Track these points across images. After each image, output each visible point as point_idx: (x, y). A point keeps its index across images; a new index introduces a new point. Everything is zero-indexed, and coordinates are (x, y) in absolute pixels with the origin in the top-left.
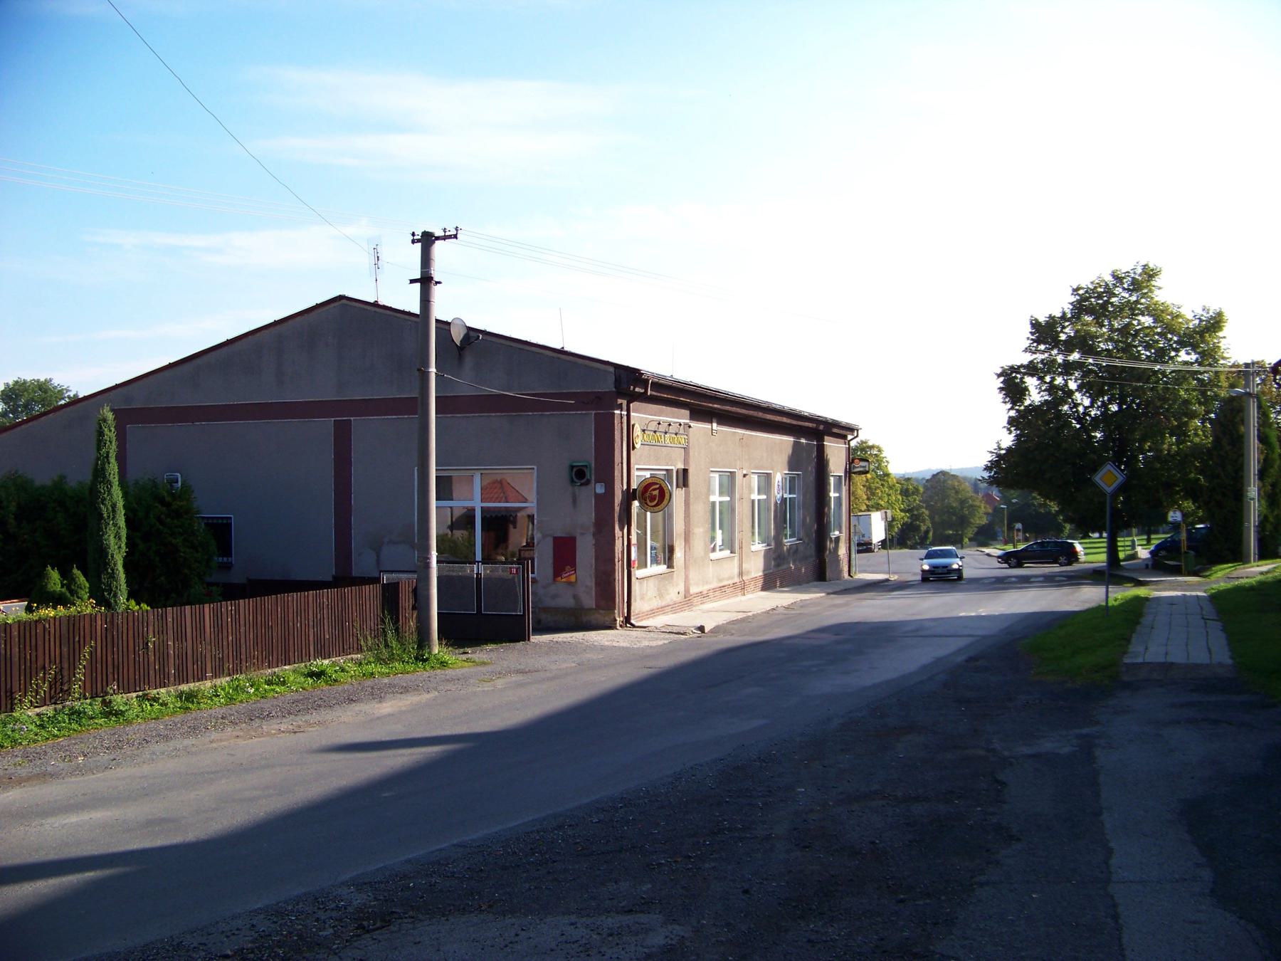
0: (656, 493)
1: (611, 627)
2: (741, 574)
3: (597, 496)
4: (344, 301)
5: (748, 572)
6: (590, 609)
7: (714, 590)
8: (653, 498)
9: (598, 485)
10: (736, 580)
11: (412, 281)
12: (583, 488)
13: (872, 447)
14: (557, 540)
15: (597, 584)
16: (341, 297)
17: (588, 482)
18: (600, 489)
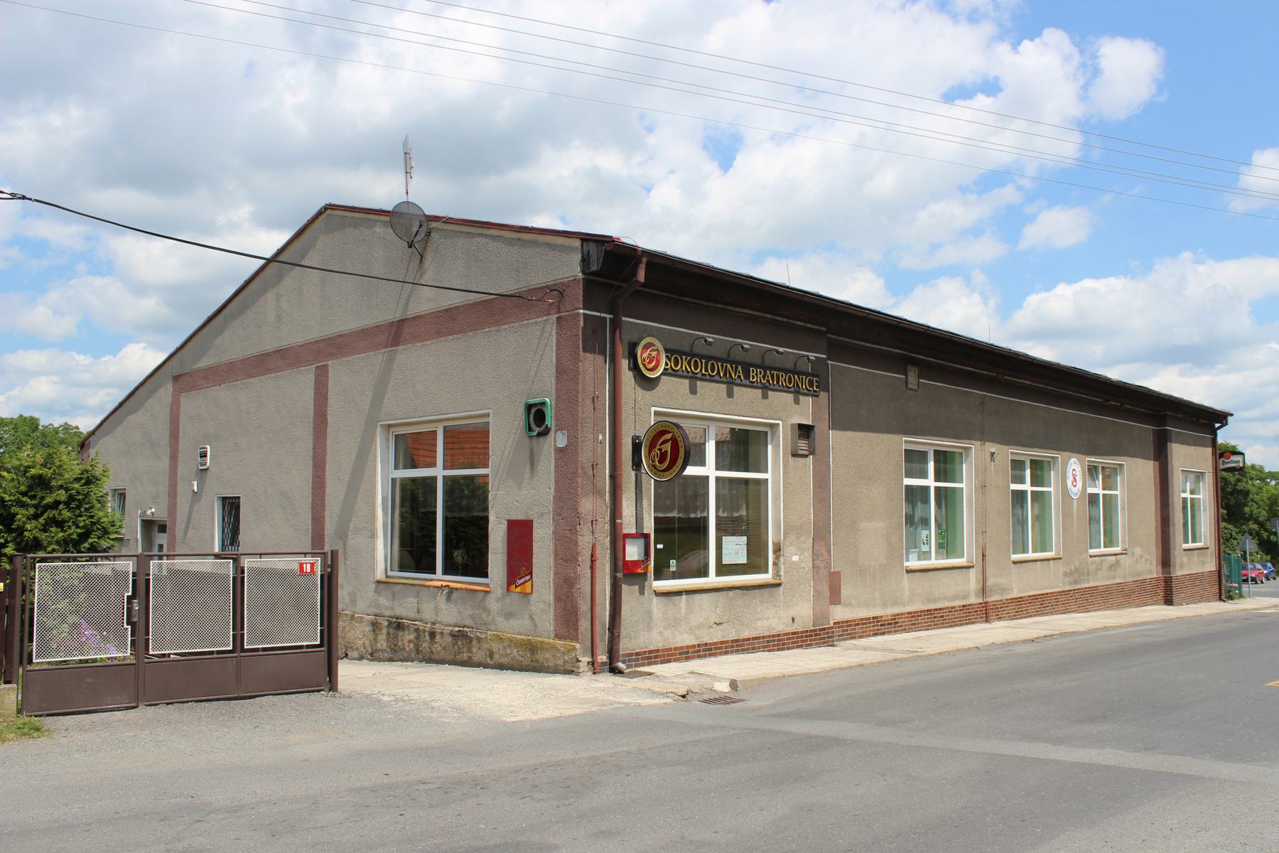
0: (668, 447)
1: (577, 674)
2: (984, 591)
3: (559, 451)
4: (329, 212)
6: (1214, 441)
7: (912, 615)
10: (973, 600)
12: (542, 439)
15: (558, 599)
16: (329, 207)
17: (545, 433)
18: (562, 441)
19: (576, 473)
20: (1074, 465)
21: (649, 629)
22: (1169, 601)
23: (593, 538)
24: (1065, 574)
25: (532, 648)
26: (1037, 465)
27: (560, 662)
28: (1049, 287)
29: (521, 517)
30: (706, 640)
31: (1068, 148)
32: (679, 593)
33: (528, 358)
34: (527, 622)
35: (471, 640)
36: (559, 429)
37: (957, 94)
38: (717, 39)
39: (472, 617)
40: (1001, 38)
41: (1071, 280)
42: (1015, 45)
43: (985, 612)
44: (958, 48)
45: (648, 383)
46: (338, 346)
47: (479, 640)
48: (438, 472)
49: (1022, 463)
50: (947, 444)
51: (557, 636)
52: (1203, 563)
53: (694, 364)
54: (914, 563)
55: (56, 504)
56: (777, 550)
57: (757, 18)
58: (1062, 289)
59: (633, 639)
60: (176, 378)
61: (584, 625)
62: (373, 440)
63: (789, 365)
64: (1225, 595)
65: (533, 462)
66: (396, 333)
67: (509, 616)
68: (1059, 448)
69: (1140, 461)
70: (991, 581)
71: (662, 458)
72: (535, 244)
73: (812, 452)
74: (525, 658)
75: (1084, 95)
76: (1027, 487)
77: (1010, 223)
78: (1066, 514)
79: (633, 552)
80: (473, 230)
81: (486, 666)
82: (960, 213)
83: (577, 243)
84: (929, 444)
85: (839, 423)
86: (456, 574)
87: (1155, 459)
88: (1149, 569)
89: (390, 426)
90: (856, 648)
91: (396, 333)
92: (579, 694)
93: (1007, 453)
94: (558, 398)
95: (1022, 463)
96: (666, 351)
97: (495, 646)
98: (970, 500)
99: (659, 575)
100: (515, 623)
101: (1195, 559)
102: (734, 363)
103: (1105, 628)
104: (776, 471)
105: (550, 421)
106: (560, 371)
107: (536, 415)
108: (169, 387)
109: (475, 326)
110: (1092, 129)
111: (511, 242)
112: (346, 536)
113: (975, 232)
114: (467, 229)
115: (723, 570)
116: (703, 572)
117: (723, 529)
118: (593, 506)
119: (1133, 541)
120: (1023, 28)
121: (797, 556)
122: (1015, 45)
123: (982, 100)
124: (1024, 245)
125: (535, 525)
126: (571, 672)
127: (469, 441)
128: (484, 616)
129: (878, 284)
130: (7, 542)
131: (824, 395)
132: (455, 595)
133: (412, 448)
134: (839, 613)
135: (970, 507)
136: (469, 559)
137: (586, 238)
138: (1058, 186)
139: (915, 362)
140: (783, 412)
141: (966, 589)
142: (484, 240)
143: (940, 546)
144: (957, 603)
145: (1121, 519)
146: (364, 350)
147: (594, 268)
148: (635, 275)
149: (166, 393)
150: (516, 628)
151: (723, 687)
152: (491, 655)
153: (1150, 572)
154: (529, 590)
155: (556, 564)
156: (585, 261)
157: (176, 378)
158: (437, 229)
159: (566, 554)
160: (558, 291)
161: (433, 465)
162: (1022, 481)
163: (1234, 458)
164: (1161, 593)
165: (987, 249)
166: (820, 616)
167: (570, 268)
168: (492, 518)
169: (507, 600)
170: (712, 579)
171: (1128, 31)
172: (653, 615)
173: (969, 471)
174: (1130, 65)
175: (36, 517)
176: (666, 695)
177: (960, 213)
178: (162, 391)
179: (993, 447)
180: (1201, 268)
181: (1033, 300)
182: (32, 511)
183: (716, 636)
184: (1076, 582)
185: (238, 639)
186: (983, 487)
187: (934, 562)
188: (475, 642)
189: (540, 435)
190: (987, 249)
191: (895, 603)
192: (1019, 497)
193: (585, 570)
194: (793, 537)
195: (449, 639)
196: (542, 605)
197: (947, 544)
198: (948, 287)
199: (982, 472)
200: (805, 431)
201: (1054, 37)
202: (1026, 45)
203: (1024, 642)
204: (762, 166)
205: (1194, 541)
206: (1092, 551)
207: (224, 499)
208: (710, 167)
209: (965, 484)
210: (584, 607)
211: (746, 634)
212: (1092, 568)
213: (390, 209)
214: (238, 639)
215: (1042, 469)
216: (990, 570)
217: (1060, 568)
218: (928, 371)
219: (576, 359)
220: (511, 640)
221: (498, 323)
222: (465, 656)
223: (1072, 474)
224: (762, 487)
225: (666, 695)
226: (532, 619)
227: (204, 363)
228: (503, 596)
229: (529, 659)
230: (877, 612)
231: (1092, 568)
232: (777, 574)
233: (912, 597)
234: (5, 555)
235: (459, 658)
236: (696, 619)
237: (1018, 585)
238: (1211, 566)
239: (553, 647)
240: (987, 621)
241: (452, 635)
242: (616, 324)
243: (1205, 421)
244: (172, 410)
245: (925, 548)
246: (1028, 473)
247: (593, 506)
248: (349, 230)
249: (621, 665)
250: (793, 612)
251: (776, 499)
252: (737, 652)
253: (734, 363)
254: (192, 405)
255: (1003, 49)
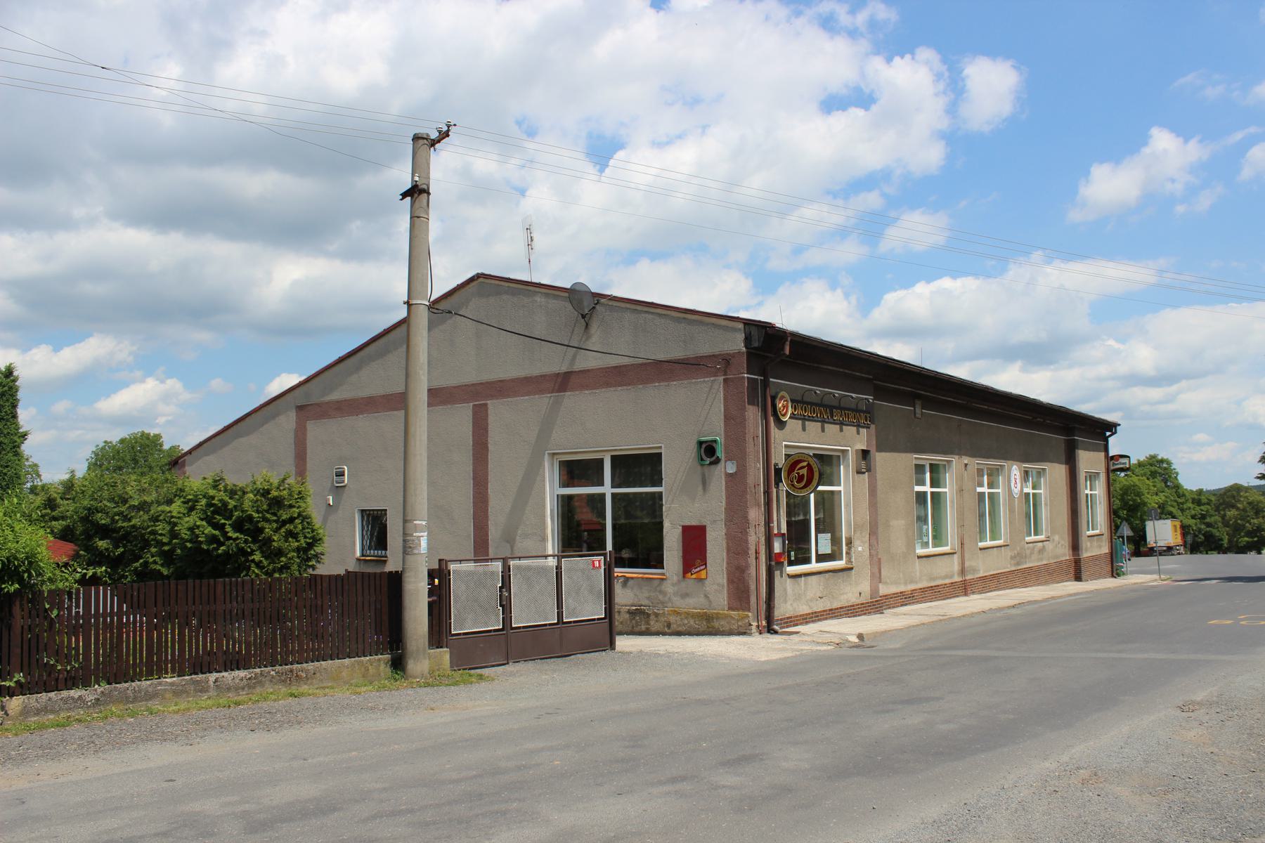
0: (804, 471)
1: (750, 634)
2: (963, 571)
3: (728, 475)
4: (481, 280)
5: (975, 570)
6: (1106, 449)
7: (923, 590)
8: (800, 478)
9: (729, 464)
10: (957, 579)
11: (823, 430)
12: (713, 467)
13: (1162, 461)
14: (687, 530)
15: (730, 581)
16: (478, 276)
17: (717, 461)
18: (731, 468)
19: (745, 492)
20: (1015, 471)
21: (785, 601)
22: (1078, 578)
23: (756, 537)
24: (1012, 558)
25: (708, 618)
26: (934, 468)
27: (735, 627)
28: (908, 284)
29: (694, 523)
30: (815, 609)
31: (932, 156)
32: (799, 576)
33: (701, 408)
34: (702, 600)
35: (648, 615)
36: (728, 459)
37: (832, 104)
38: (607, 46)
39: (648, 598)
40: (877, 53)
41: (929, 280)
42: (889, 60)
43: (964, 588)
44: (834, 60)
45: (781, 424)
46: (501, 389)
47: (657, 615)
48: (607, 489)
49: (923, 466)
50: (937, 458)
51: (730, 608)
52: (1100, 547)
53: (813, 410)
54: (920, 551)
55: (291, 520)
56: (849, 543)
57: (646, 29)
58: (921, 288)
59: (783, 609)
60: (300, 408)
61: (753, 599)
62: (540, 465)
63: (853, 406)
64: (1115, 573)
65: (704, 483)
66: (563, 382)
67: (685, 595)
68: (1005, 458)
69: (1056, 465)
70: (967, 564)
71: (800, 478)
72: (702, 323)
73: (869, 470)
74: (703, 625)
75: (952, 110)
76: (927, 488)
77: (871, 227)
78: (1012, 511)
79: (777, 547)
80: (639, 308)
81: (664, 634)
82: (834, 216)
83: (741, 326)
84: (927, 458)
85: (880, 448)
86: (624, 567)
87: (1067, 463)
88: (1065, 553)
89: (554, 454)
90: (897, 615)
91: (563, 382)
92: (758, 649)
93: (974, 463)
94: (727, 436)
95: (923, 466)
96: (792, 401)
97: (672, 619)
98: (952, 502)
99: (791, 563)
100: (691, 601)
101: (1095, 544)
102: (825, 406)
103: (1053, 598)
104: (846, 485)
105: (720, 452)
106: (727, 418)
107: (708, 450)
108: (292, 415)
109: (646, 381)
110: (957, 140)
111: (678, 320)
112: (514, 540)
113: (842, 233)
114: (628, 306)
115: (821, 558)
116: (807, 561)
117: (818, 531)
118: (755, 515)
119: (1054, 530)
120: (894, 45)
121: (860, 547)
122: (889, 60)
123: (857, 113)
124: (884, 246)
125: (708, 529)
126: (744, 634)
127: (638, 467)
128: (661, 597)
129: (745, 285)
130: (253, 551)
131: (873, 426)
132: (630, 583)
133: (576, 471)
134: (884, 590)
135: (952, 507)
136: (650, 556)
137: (748, 323)
138: (915, 192)
139: (919, 397)
140: (852, 440)
141: (948, 571)
142: (650, 316)
143: (935, 537)
144: (947, 581)
145: (1044, 513)
146: (528, 394)
147: (756, 344)
148: (783, 349)
149: (287, 421)
150: (694, 603)
151: (854, 639)
152: (669, 625)
153: (1064, 555)
154: (703, 576)
155: (728, 558)
156: (748, 340)
157: (300, 408)
158: (603, 304)
159: (737, 548)
160: (726, 361)
161: (601, 484)
162: (923, 483)
163: (1122, 460)
164: (1072, 571)
165: (850, 252)
166: (874, 591)
167: (736, 343)
168: (666, 524)
169: (683, 584)
170: (814, 566)
171: (992, 52)
172: (795, 593)
173: (951, 478)
174: (993, 84)
175: (276, 530)
176: (828, 644)
177: (834, 216)
178: (282, 419)
179: (966, 460)
180: (1048, 269)
181: (890, 298)
182: (275, 525)
183: (819, 606)
184: (1018, 564)
185: (560, 615)
186: (961, 491)
187: (931, 550)
188: (652, 617)
189: (711, 463)
190: (850, 252)
191: (911, 582)
192: (921, 497)
193: (752, 560)
194: (858, 534)
195: (627, 616)
196: (716, 587)
197: (938, 538)
198: (813, 287)
199: (960, 479)
200: (865, 454)
201: (925, 54)
202: (897, 60)
203: (1009, 607)
204: (640, 165)
205: (1036, 534)
206: (1028, 539)
207: (362, 511)
208: (591, 169)
209: (946, 490)
210: (753, 587)
211: (835, 605)
212: (1028, 552)
213: (568, 286)
214: (560, 615)
215: (938, 472)
216: (967, 556)
217: (1007, 553)
218: (928, 403)
219: (744, 409)
220: (688, 614)
221: (669, 379)
222: (643, 628)
223: (1014, 478)
224: (836, 497)
225: (828, 644)
226: (706, 596)
227: (335, 396)
228: (679, 581)
229: (708, 626)
230: (902, 588)
231: (1028, 552)
232: (849, 561)
233: (921, 577)
234: (253, 561)
235: (637, 629)
236: (810, 594)
237: (983, 567)
238: (1105, 549)
239: (726, 616)
240: (966, 595)
241: (629, 612)
242: (766, 384)
243: (1099, 430)
244: (296, 436)
245: (925, 539)
246: (928, 475)
247: (755, 515)
248: (505, 297)
249: (776, 627)
250: (860, 589)
251: (847, 505)
252: (832, 618)
253: (825, 406)
254: (316, 431)
255: (877, 63)
